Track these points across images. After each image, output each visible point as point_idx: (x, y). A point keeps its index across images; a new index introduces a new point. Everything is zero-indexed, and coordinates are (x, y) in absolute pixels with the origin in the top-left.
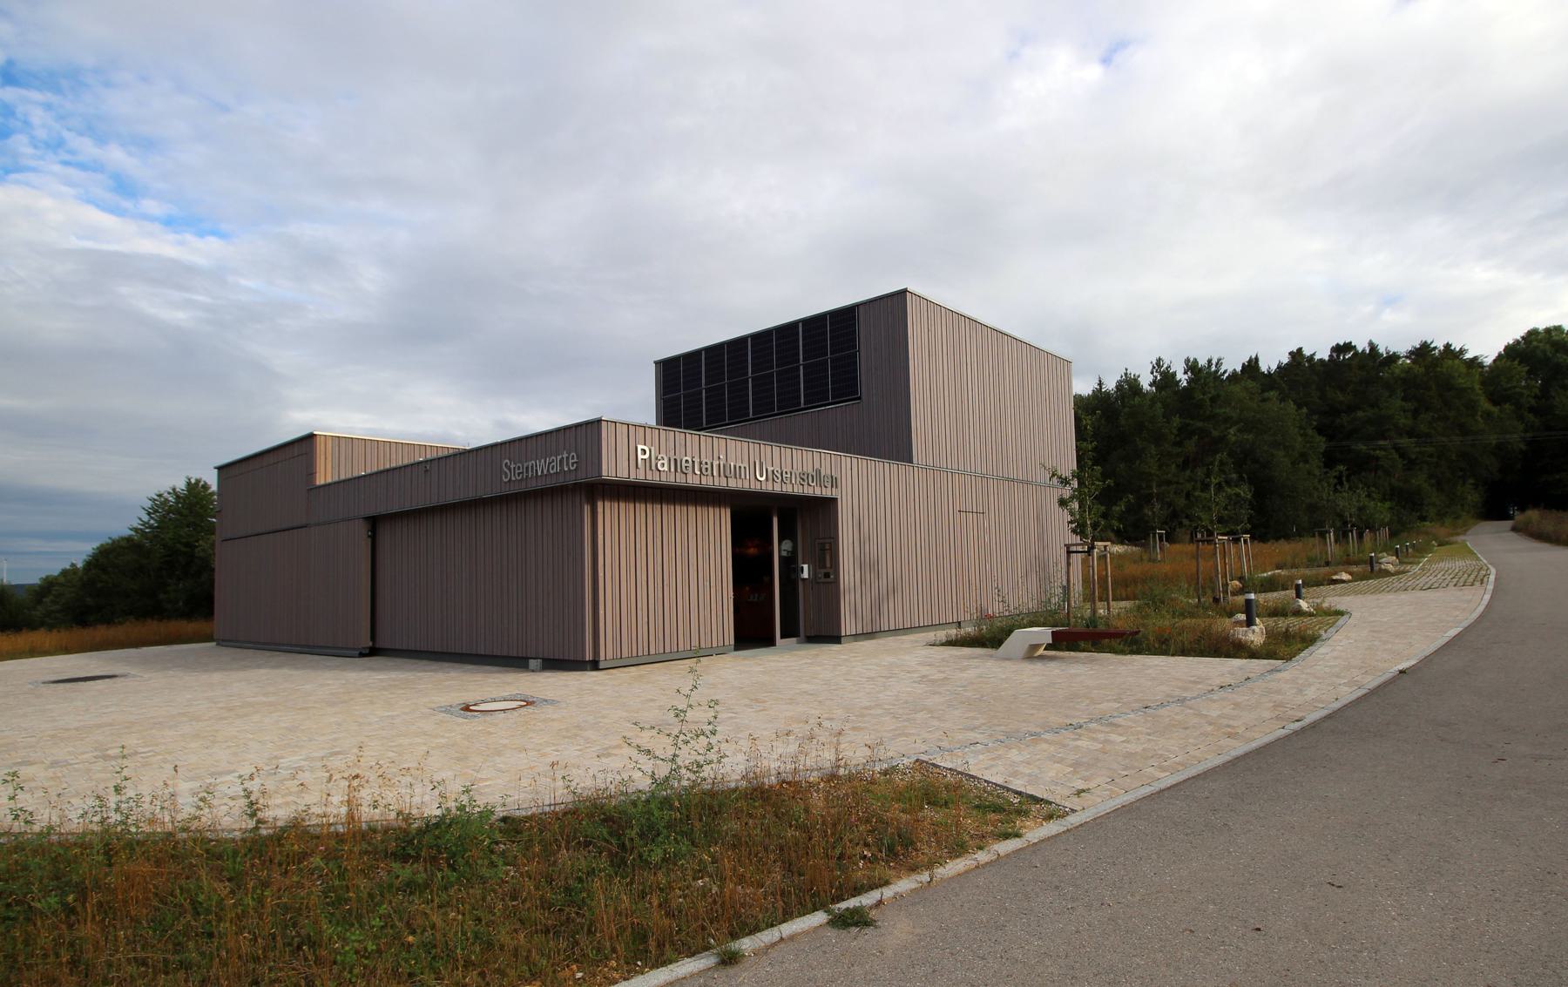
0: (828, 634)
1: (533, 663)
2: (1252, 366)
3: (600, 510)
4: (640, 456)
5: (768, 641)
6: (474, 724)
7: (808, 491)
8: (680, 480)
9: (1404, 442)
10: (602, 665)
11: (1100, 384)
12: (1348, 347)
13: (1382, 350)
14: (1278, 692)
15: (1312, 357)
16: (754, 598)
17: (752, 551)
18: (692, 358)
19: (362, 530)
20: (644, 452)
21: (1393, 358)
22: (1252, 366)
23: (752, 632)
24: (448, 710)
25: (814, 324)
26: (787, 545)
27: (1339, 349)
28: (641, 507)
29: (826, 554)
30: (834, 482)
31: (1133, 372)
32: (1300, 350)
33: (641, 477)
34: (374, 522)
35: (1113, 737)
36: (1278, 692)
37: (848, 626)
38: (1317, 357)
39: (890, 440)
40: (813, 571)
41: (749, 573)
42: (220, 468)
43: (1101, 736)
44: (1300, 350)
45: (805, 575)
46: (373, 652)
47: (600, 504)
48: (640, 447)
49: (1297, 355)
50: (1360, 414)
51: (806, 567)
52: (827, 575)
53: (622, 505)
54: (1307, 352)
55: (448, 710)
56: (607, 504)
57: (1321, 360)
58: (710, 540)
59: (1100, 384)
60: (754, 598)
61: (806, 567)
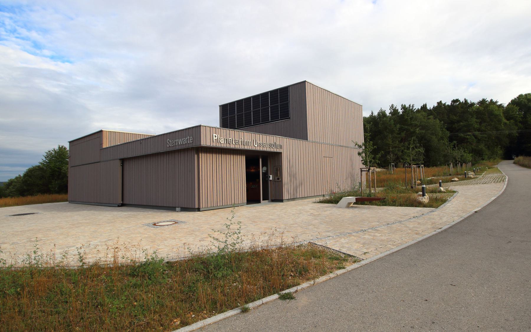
0: (279, 199)
1: (177, 209)
2: (424, 107)
3: (200, 156)
4: (214, 138)
5: (258, 201)
6: (157, 230)
7: (272, 150)
8: (228, 146)
9: (477, 133)
10: (201, 210)
11: (372, 113)
12: (457, 100)
13: (469, 102)
14: (433, 219)
15: (445, 104)
16: (253, 187)
17: (253, 170)
18: (232, 104)
19: (119, 163)
20: (216, 136)
21: (473, 104)
22: (424, 107)
23: (253, 198)
24: (148, 225)
25: (274, 92)
26: (265, 168)
27: (454, 101)
28: (214, 155)
29: (278, 172)
30: (281, 147)
31: (383, 109)
32: (441, 102)
33: (215, 145)
34: (123, 161)
35: (377, 234)
36: (433, 219)
37: (286, 196)
38: (446, 104)
39: (300, 132)
40: (274, 177)
41: (252, 178)
42: (70, 142)
43: (372, 234)
44: (441, 102)
45: (271, 179)
46: (123, 205)
47: (200, 154)
48: (214, 135)
49: (440, 103)
50: (461, 123)
51: (271, 176)
52: (278, 179)
53: (208, 155)
54: (443, 102)
55: (148, 225)
56: (203, 154)
57: (448, 105)
58: (238, 167)
59: (372, 113)
60: (253, 187)
61: (271, 176)
